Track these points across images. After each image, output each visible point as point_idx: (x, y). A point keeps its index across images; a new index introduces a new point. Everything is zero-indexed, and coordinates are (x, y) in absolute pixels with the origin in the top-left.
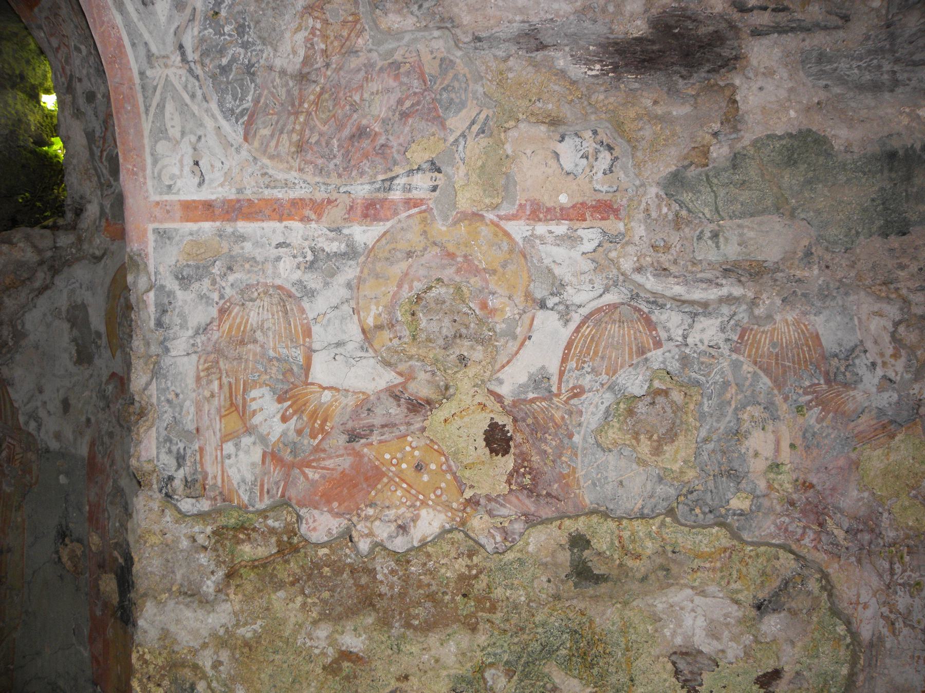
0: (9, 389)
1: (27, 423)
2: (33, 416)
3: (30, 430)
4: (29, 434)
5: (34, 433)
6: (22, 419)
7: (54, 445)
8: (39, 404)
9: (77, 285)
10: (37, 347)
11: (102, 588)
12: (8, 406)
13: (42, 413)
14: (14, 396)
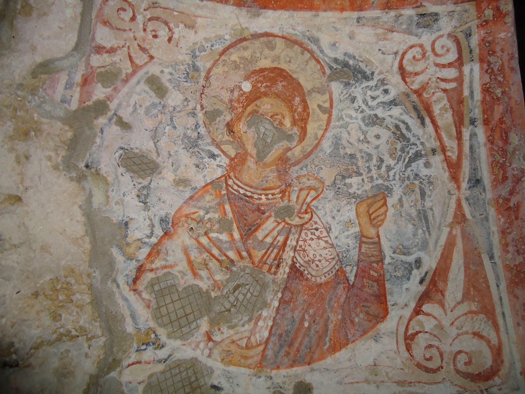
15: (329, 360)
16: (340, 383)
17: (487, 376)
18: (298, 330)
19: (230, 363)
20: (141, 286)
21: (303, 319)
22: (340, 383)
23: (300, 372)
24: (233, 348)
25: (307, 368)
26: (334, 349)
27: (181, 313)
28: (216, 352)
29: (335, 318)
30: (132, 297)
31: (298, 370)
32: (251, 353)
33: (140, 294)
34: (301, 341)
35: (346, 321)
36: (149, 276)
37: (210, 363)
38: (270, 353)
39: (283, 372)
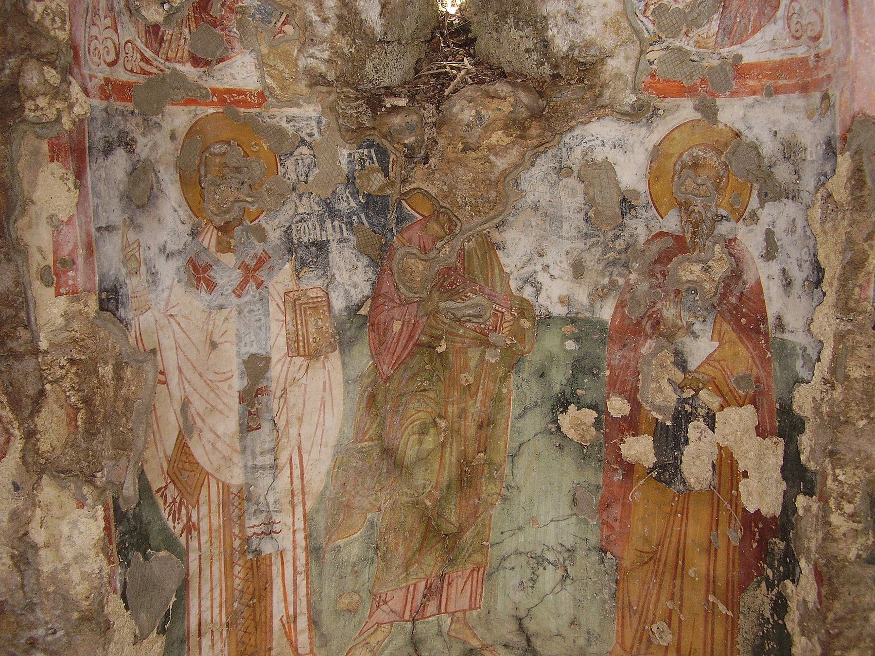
0: (500, 253)
1: (520, 289)
2: (530, 280)
3: (525, 296)
4: (523, 300)
5: (531, 299)
6: (513, 285)
7: (559, 310)
8: (539, 267)
9: (598, 142)
10: (535, 208)
11: (623, 452)
12: (497, 271)
13: (543, 278)
14: (504, 260)
15: (751, 40)
16: (756, 53)
17: (611, 653)
18: (734, 24)
19: (699, 47)
20: (649, 13)
21: (736, 17)
22: (756, 53)
23: (736, 49)
24: (700, 39)
25: (740, 46)
26: (754, 32)
27: (671, 24)
28: (691, 42)
29: (754, 12)
30: (644, 19)
31: (734, 47)
32: (709, 41)
33: (648, 17)
34: (681, 596)
35: (761, 13)
36: (652, 7)
37: (688, 48)
38: (719, 39)
39: (727, 49)
